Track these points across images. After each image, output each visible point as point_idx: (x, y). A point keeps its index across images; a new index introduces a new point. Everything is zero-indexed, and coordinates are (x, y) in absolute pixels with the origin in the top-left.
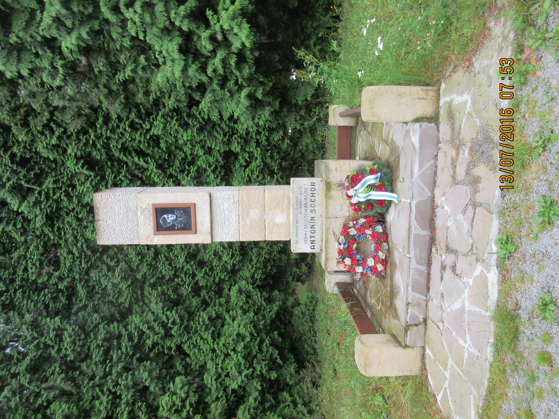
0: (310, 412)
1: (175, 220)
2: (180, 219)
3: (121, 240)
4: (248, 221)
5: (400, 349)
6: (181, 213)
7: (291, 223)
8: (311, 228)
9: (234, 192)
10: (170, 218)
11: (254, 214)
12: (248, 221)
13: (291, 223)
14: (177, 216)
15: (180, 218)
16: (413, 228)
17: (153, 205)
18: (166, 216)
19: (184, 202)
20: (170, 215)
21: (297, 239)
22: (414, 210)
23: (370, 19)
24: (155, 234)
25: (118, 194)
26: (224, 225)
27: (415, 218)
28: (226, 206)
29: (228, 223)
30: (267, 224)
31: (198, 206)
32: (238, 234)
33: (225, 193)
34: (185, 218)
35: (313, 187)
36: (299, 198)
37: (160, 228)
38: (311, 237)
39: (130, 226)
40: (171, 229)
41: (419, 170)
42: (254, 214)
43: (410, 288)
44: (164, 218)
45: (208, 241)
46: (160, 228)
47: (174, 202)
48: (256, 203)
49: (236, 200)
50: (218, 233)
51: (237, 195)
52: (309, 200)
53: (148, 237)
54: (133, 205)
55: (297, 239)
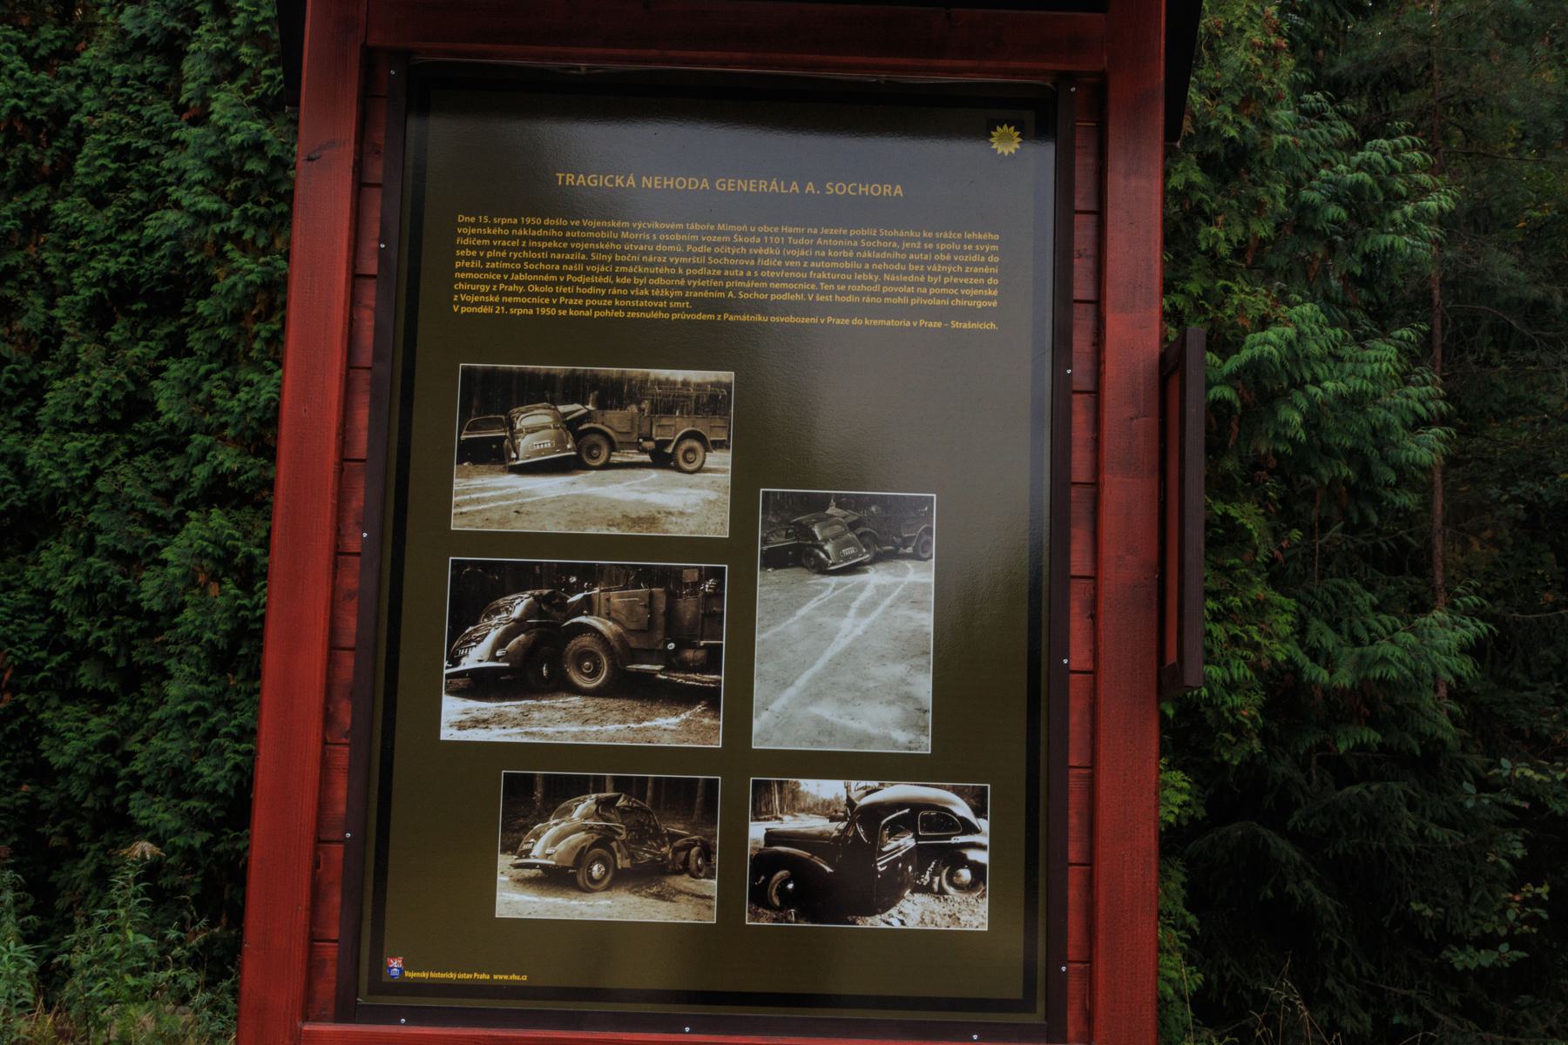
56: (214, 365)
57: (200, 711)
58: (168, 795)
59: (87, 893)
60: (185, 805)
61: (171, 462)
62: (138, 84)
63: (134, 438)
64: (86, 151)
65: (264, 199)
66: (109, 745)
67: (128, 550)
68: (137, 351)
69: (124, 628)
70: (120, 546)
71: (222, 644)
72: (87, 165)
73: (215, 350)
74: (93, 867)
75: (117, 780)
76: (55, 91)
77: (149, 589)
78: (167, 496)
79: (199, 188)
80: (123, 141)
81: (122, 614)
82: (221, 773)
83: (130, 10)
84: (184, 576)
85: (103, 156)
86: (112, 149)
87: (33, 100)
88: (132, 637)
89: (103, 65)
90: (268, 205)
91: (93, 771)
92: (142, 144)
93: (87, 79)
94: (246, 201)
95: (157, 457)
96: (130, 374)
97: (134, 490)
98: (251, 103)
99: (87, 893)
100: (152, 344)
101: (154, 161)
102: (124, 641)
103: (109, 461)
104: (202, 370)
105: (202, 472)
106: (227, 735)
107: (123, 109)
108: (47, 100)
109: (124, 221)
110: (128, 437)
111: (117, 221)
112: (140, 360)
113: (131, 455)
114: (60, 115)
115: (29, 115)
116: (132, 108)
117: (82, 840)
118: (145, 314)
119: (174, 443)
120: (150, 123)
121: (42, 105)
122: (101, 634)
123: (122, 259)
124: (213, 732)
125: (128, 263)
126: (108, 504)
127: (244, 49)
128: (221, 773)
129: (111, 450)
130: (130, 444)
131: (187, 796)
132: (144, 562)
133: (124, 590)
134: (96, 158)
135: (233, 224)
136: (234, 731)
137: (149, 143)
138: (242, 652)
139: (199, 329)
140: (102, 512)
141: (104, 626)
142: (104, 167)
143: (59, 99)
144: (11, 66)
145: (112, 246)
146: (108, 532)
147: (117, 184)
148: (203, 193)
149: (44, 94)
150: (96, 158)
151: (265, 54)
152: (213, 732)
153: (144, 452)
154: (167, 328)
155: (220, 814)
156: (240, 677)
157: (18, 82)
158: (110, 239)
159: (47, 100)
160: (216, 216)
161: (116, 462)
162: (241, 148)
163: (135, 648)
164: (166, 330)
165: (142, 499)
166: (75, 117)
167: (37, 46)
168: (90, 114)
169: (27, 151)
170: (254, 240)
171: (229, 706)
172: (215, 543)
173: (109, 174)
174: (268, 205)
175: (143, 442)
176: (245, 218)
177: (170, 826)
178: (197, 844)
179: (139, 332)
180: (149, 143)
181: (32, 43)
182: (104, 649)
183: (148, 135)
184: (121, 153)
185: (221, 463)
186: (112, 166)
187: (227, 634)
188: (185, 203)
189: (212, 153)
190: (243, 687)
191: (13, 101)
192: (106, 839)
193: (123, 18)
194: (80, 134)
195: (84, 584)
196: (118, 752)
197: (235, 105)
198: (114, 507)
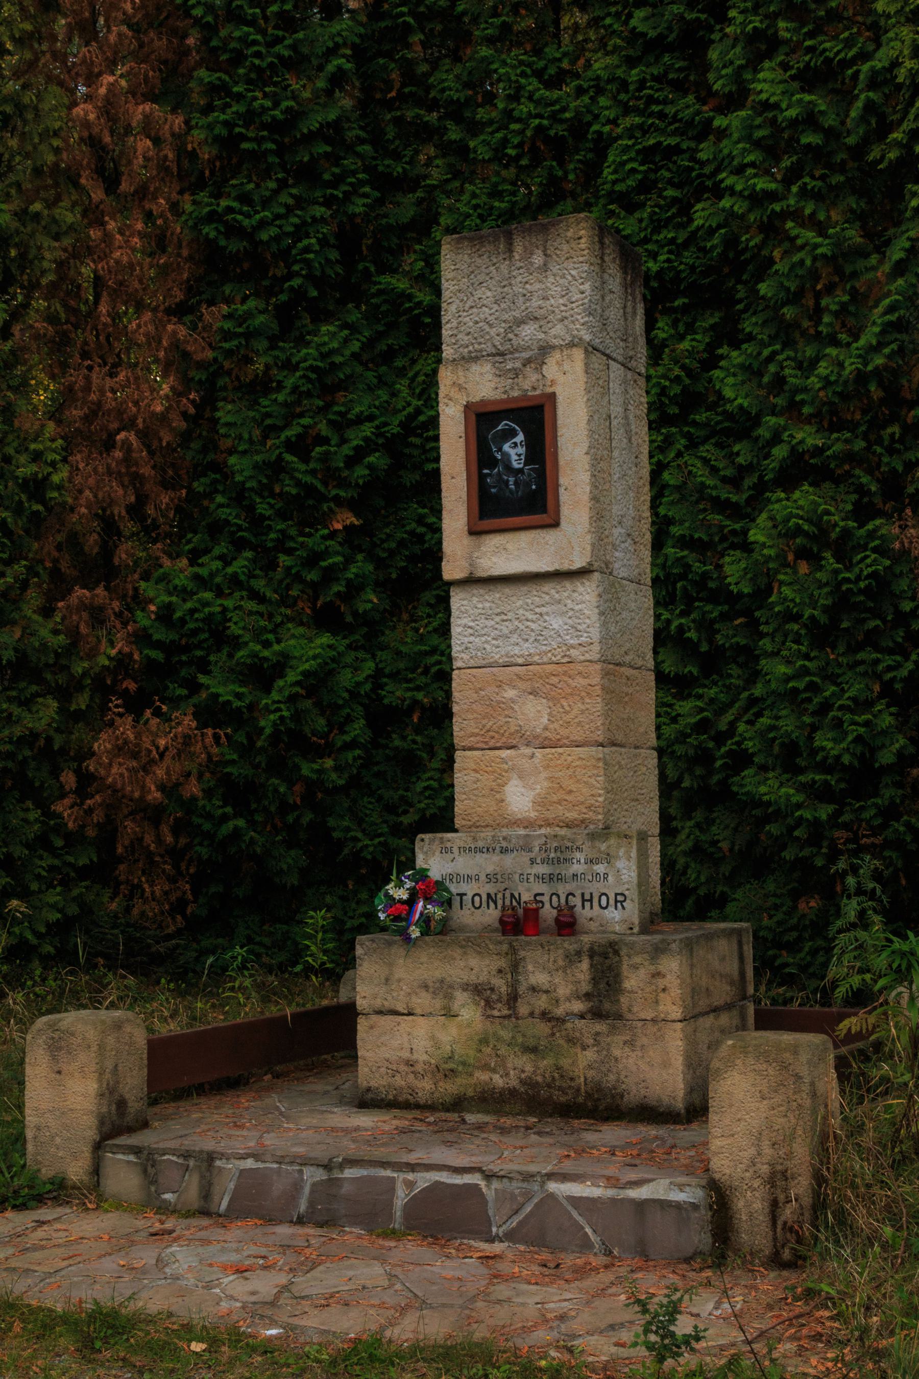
0: (19, 952)
1: (508, 468)
2: (512, 480)
3: (453, 308)
4: (510, 693)
5: (92, 1134)
6: (528, 484)
7: (505, 832)
8: (489, 895)
9: (596, 648)
10: (514, 452)
11: (534, 714)
12: (510, 693)
13: (505, 832)
14: (520, 471)
15: (516, 483)
16: (410, 1176)
17: (552, 397)
18: (520, 437)
19: (562, 490)
20: (521, 450)
21: (455, 850)
22: (458, 1180)
23: (336, 768)
24: (468, 407)
25: (587, 287)
26: (498, 619)
27: (437, 1183)
28: (556, 623)
29: (506, 631)
30: (505, 753)
31: (550, 536)
32: (472, 663)
33: (595, 617)
34: (518, 497)
35: (612, 902)
36: (578, 855)
37: (484, 421)
38: (461, 895)
39: (493, 332)
40: (483, 456)
41: (576, 1201)
42: (534, 714)
43: (250, 1163)
44: (514, 434)
45: (451, 570)
46: (484, 421)
47: (562, 462)
48: (567, 718)
49: (574, 653)
50: (475, 599)
51: (588, 657)
52: (569, 887)
53: (461, 388)
54: (555, 337)
55: (455, 850)
56: (778, 347)
57: (813, 687)
58: (779, 771)
59: (687, 867)
60: (802, 778)
61: (736, 448)
62: (657, 86)
63: (692, 430)
64: (611, 158)
65: (817, 173)
66: (702, 726)
67: (705, 538)
68: (685, 345)
69: (704, 613)
70: (696, 536)
71: (823, 619)
72: (615, 172)
73: (773, 332)
74: (690, 844)
75: (714, 760)
76: (572, 105)
77: (734, 571)
78: (735, 482)
79: (750, 171)
80: (652, 142)
81: (700, 600)
82: (844, 745)
83: (640, 14)
84: (777, 556)
85: (631, 160)
86: (638, 152)
87: (554, 117)
88: (713, 622)
89: (619, 73)
90: (823, 178)
91: (691, 752)
92: (672, 141)
93: (600, 91)
94: (802, 177)
95: (719, 445)
96: (683, 367)
97: (702, 475)
98: (793, 78)
99: (687, 867)
100: (698, 337)
101: (687, 155)
102: (707, 627)
103: (672, 455)
104: (766, 352)
105: (780, 452)
106: (841, 708)
107: (640, 112)
108: (567, 115)
109: (659, 221)
110: (686, 429)
111: (652, 221)
112: (691, 353)
113: (693, 444)
114: (578, 128)
115: (552, 133)
116: (656, 108)
117: (675, 818)
118: (685, 309)
119: (742, 425)
120: (675, 119)
121: (562, 121)
122: (683, 621)
123: (662, 258)
124: (825, 707)
125: (668, 261)
126: (676, 496)
127: (782, 24)
128: (844, 745)
129: (671, 444)
130: (688, 436)
131: (802, 771)
132: (720, 548)
133: (705, 576)
134: (623, 164)
135: (792, 202)
136: (849, 703)
137: (678, 140)
138: (844, 625)
139: (755, 313)
140: (672, 503)
141: (683, 614)
142: (633, 171)
143: (578, 113)
144: (530, 88)
145: (649, 247)
146: (682, 522)
147: (646, 186)
148: (755, 175)
149: (564, 109)
150: (623, 164)
151: (803, 25)
152: (825, 707)
153: (704, 442)
154: (712, 318)
155: (843, 785)
156: (841, 650)
157: (538, 102)
158: (646, 240)
159: (567, 115)
160: (772, 196)
161: (679, 454)
162: (794, 123)
163: (719, 631)
164: (711, 321)
165: (715, 487)
166: (595, 127)
167: (545, 68)
168: (609, 122)
169: (552, 167)
170: (813, 214)
171: (833, 679)
172: (809, 521)
173: (639, 177)
174: (823, 178)
175: (702, 433)
176: (804, 193)
177: (794, 800)
178: (824, 817)
179: (681, 328)
180: (678, 140)
181: (541, 64)
182: (688, 635)
183: (674, 133)
184: (647, 155)
185: (802, 442)
186: (642, 168)
187: (826, 609)
188: (738, 188)
189: (760, 133)
190: (843, 660)
191: (537, 121)
192: (699, 815)
193: (633, 22)
194: (602, 145)
195: (661, 575)
196: (713, 733)
197: (781, 82)
198: (683, 498)
